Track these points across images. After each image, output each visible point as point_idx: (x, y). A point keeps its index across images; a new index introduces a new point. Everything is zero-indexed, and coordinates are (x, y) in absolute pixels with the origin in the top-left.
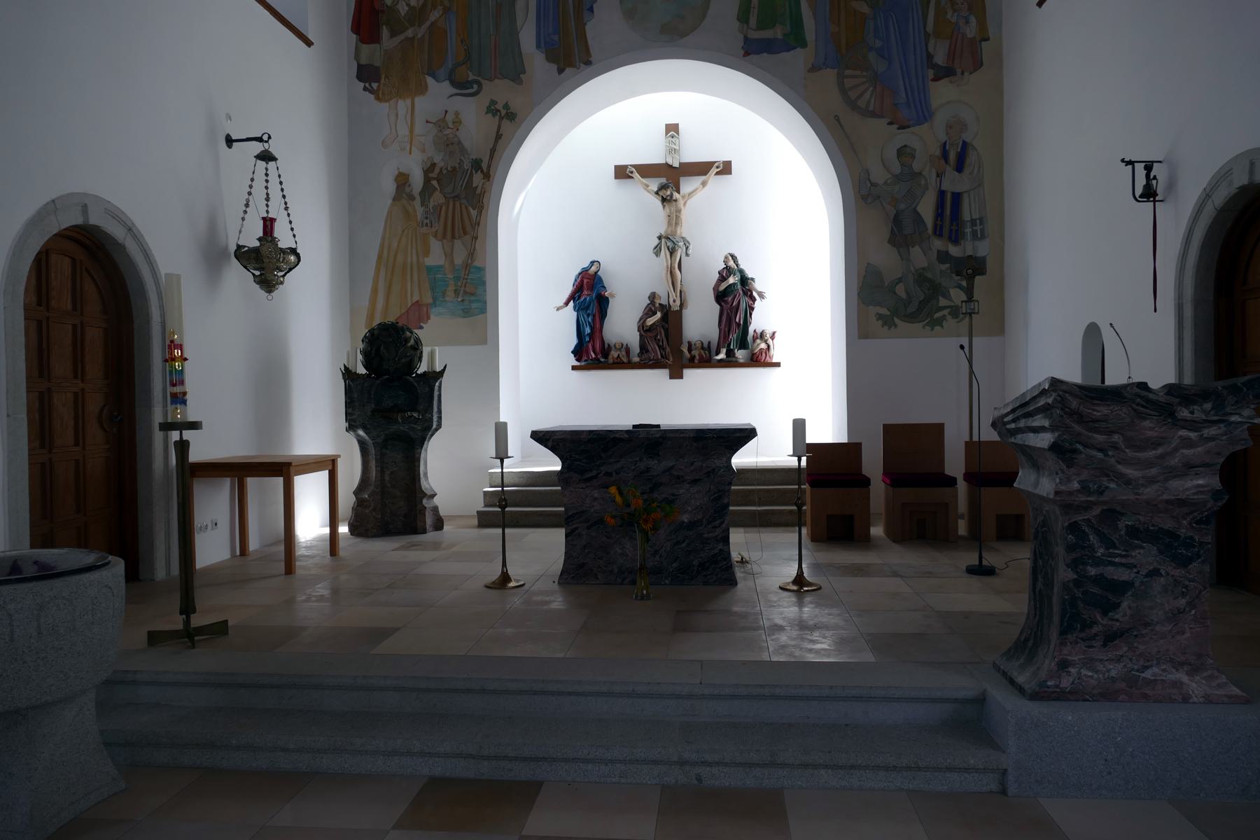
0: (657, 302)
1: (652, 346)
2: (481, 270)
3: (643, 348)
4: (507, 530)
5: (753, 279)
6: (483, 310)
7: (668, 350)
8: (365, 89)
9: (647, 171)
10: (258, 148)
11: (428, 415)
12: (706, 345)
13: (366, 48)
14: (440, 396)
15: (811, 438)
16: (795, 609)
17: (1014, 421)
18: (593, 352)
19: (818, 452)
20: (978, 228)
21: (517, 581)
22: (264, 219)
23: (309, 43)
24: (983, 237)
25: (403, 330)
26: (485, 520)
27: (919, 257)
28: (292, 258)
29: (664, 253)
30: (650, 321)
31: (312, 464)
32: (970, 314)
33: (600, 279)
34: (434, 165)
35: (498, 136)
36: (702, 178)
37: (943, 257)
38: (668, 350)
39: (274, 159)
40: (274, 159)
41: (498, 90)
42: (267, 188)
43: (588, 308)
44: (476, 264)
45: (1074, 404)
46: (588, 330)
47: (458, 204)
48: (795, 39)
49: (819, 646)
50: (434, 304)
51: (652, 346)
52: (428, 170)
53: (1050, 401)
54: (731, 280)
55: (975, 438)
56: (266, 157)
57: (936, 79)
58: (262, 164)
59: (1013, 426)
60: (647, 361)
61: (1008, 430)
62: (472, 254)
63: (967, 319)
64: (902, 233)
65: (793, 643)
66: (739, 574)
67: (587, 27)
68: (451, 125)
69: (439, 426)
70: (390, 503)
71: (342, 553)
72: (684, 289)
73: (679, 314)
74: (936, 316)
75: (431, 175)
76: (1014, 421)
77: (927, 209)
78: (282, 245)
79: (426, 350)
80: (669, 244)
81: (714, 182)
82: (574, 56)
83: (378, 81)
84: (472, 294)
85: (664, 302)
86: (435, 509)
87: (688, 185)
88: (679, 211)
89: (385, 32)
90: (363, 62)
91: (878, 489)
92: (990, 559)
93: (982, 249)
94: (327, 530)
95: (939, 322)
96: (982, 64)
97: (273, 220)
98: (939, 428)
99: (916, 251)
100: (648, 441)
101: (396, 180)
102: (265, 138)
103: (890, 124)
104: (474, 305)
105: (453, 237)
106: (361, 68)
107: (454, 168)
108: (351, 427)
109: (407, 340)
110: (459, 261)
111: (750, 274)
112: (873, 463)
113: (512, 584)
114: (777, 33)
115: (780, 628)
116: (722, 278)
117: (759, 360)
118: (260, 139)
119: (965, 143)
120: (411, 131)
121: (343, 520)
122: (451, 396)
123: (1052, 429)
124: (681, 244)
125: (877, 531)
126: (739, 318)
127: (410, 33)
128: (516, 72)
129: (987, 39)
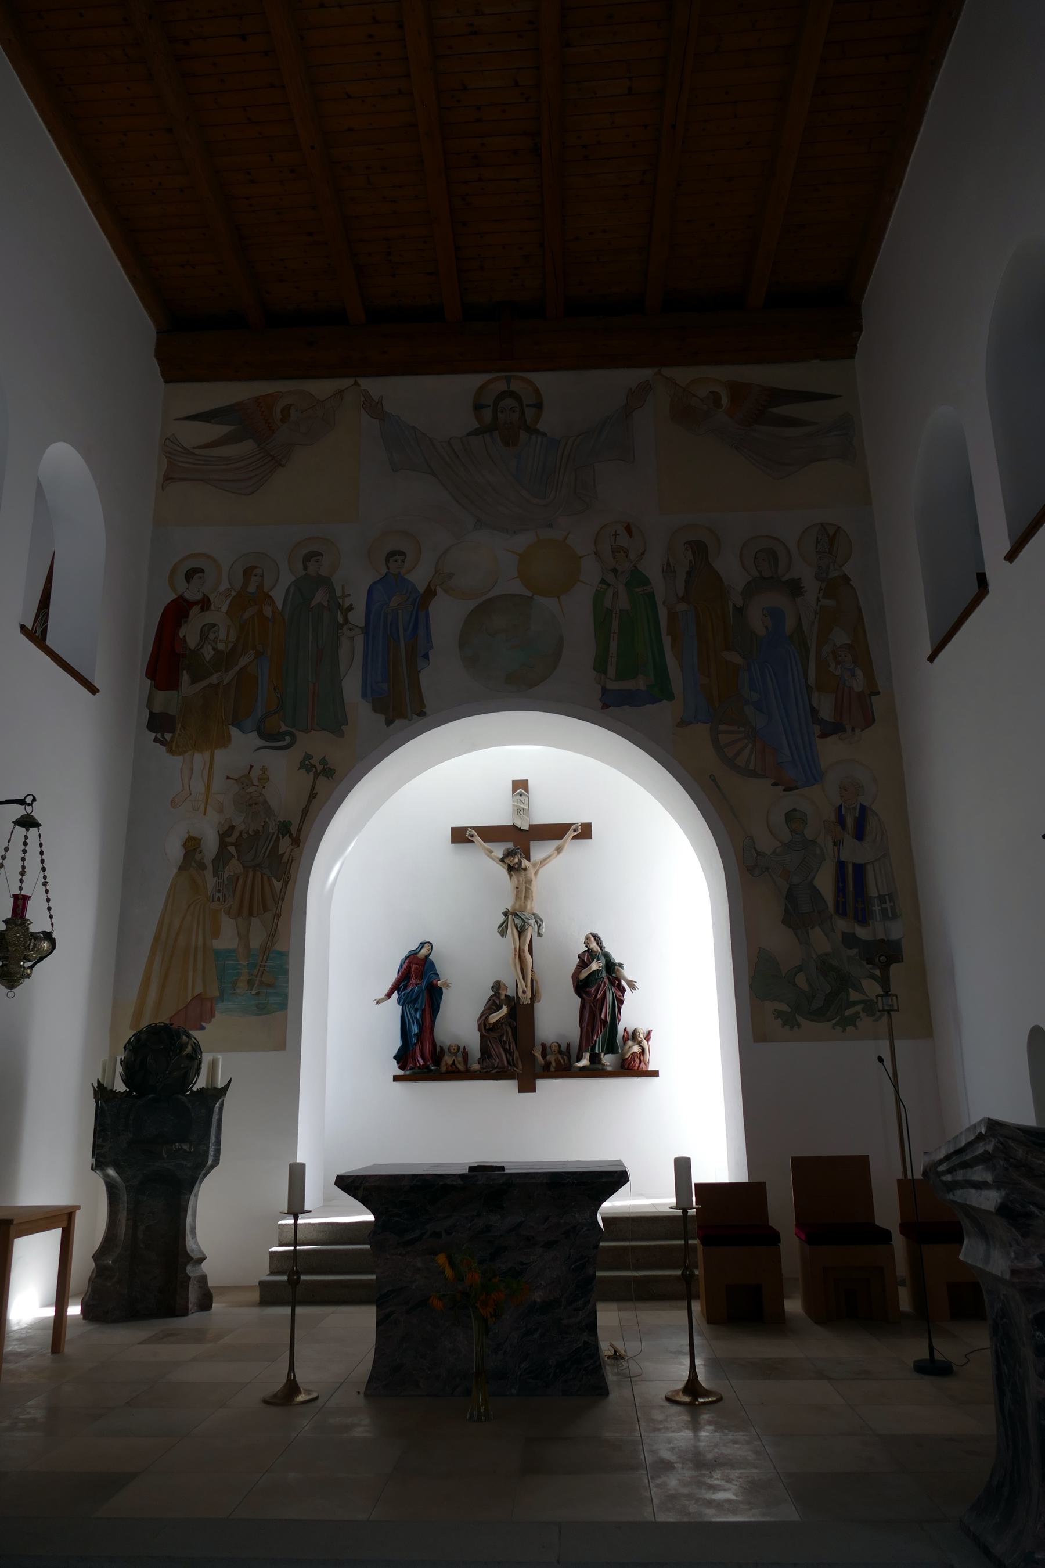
0: (503, 993)
1: (497, 1050)
2: (284, 955)
3: (485, 1052)
4: (299, 1310)
5: (620, 965)
6: (283, 1006)
7: (516, 1054)
8: (156, 740)
9: (489, 834)
10: (19, 811)
12: (564, 1048)
13: (161, 695)
14: (220, 1121)
15: (700, 1175)
16: (688, 1434)
17: (950, 1171)
18: (421, 1057)
19: (712, 1193)
20: (888, 905)
21: (308, 1392)
22: (15, 897)
23: (94, 690)
24: (895, 917)
26: (269, 1295)
27: (821, 941)
28: (45, 945)
29: (512, 932)
30: (494, 1018)
31: (38, 1220)
32: (889, 1012)
33: (432, 965)
34: (232, 828)
35: (313, 795)
36: (556, 843)
37: (849, 940)
38: (516, 1054)
39: (37, 825)
40: (37, 825)
41: (315, 743)
42: (23, 859)
43: (415, 1001)
44: (278, 947)
45: (1020, 1152)
46: (415, 1029)
47: (258, 874)
48: (661, 691)
49: (721, 1496)
50: (221, 998)
51: (497, 1050)
52: (225, 834)
53: (990, 1148)
54: (594, 966)
55: (910, 1177)
56: (28, 822)
57: (824, 735)
58: (20, 831)
59: (948, 1178)
60: (488, 1068)
61: (945, 1183)
62: (273, 935)
63: (885, 1019)
64: (798, 912)
65: (685, 1490)
66: (611, 1378)
67: (421, 676)
68: (256, 783)
69: (216, 1161)
70: (141, 1272)
71: (68, 1349)
72: (536, 977)
73: (530, 1009)
74: (847, 1013)
75: (229, 840)
76: (950, 1171)
77: (825, 882)
78: (34, 928)
79: (206, 1058)
80: (518, 922)
81: (572, 849)
82: (405, 707)
83: (172, 731)
84: (270, 985)
85: (511, 993)
86: (203, 1279)
87: (539, 851)
88: (529, 882)
89: (185, 677)
90: (157, 709)
91: (791, 1247)
92: (946, 1350)
93: (896, 931)
94: (51, 1312)
95: (852, 1021)
96: (874, 720)
97: (26, 898)
98: (862, 1163)
99: (816, 934)
100: (488, 1189)
101: (185, 845)
102: (29, 800)
103: (775, 784)
105: (251, 914)
106: (152, 716)
107: (257, 832)
108: (98, 1165)
109: (183, 1047)
110: (255, 943)
111: (617, 960)
112: (781, 1209)
113: (301, 1398)
114: (640, 684)
115: (666, 1466)
116: (583, 964)
117: (633, 1067)
118: (21, 802)
119: (863, 808)
120: (208, 787)
121: (76, 1295)
122: (234, 1122)
123: (997, 1185)
124: (532, 922)
125: (793, 1306)
126: (605, 1013)
127: (214, 679)
128: (336, 723)
129: (878, 693)
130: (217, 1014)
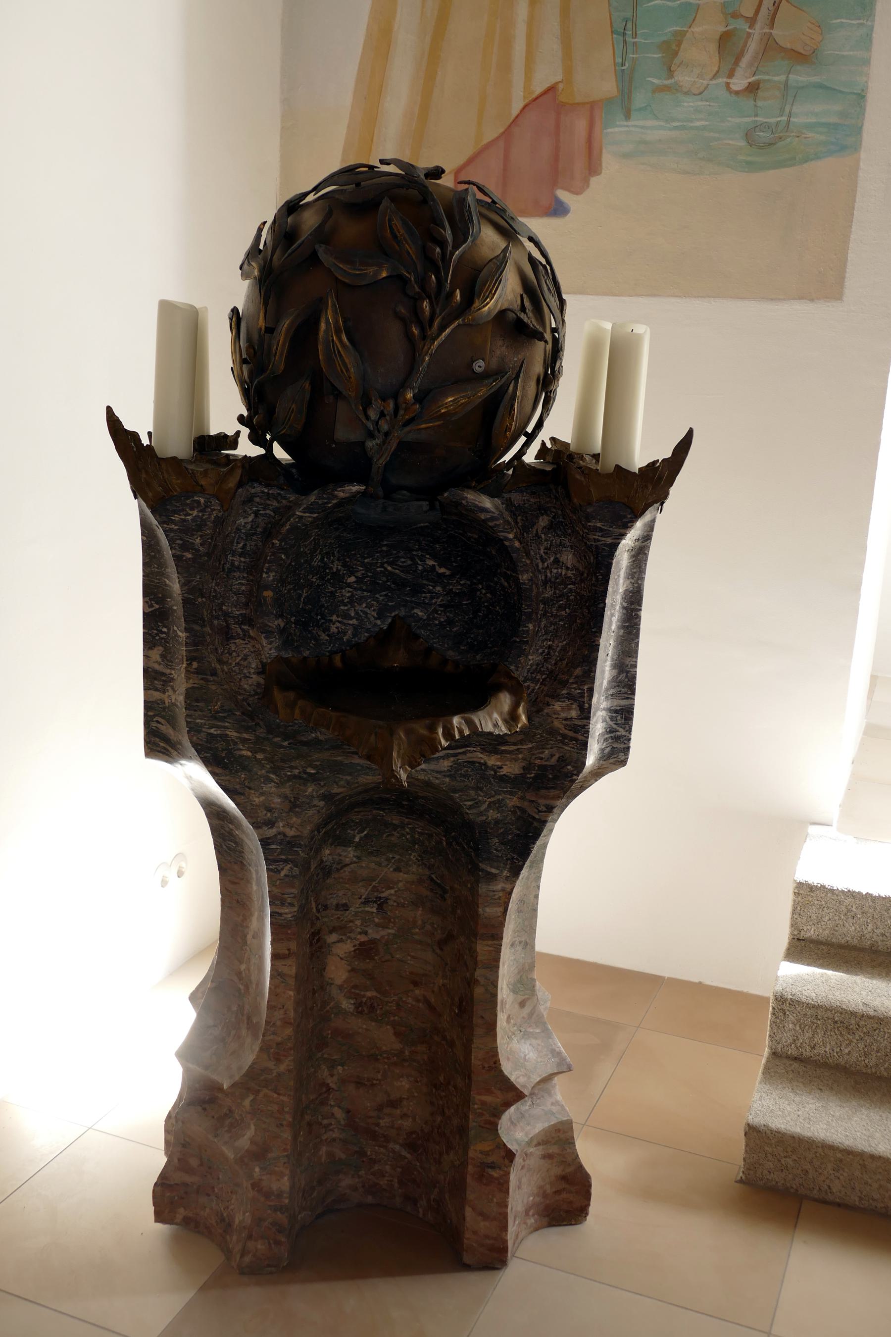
11: (562, 711)
25: (459, 214)
69: (617, 753)
79: (584, 322)
84: (800, 57)
104: (805, 113)
109: (478, 279)
130: (609, 162)
